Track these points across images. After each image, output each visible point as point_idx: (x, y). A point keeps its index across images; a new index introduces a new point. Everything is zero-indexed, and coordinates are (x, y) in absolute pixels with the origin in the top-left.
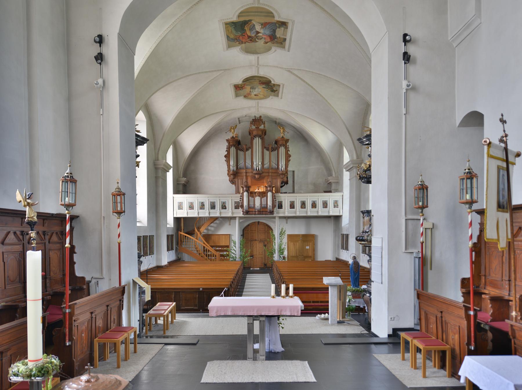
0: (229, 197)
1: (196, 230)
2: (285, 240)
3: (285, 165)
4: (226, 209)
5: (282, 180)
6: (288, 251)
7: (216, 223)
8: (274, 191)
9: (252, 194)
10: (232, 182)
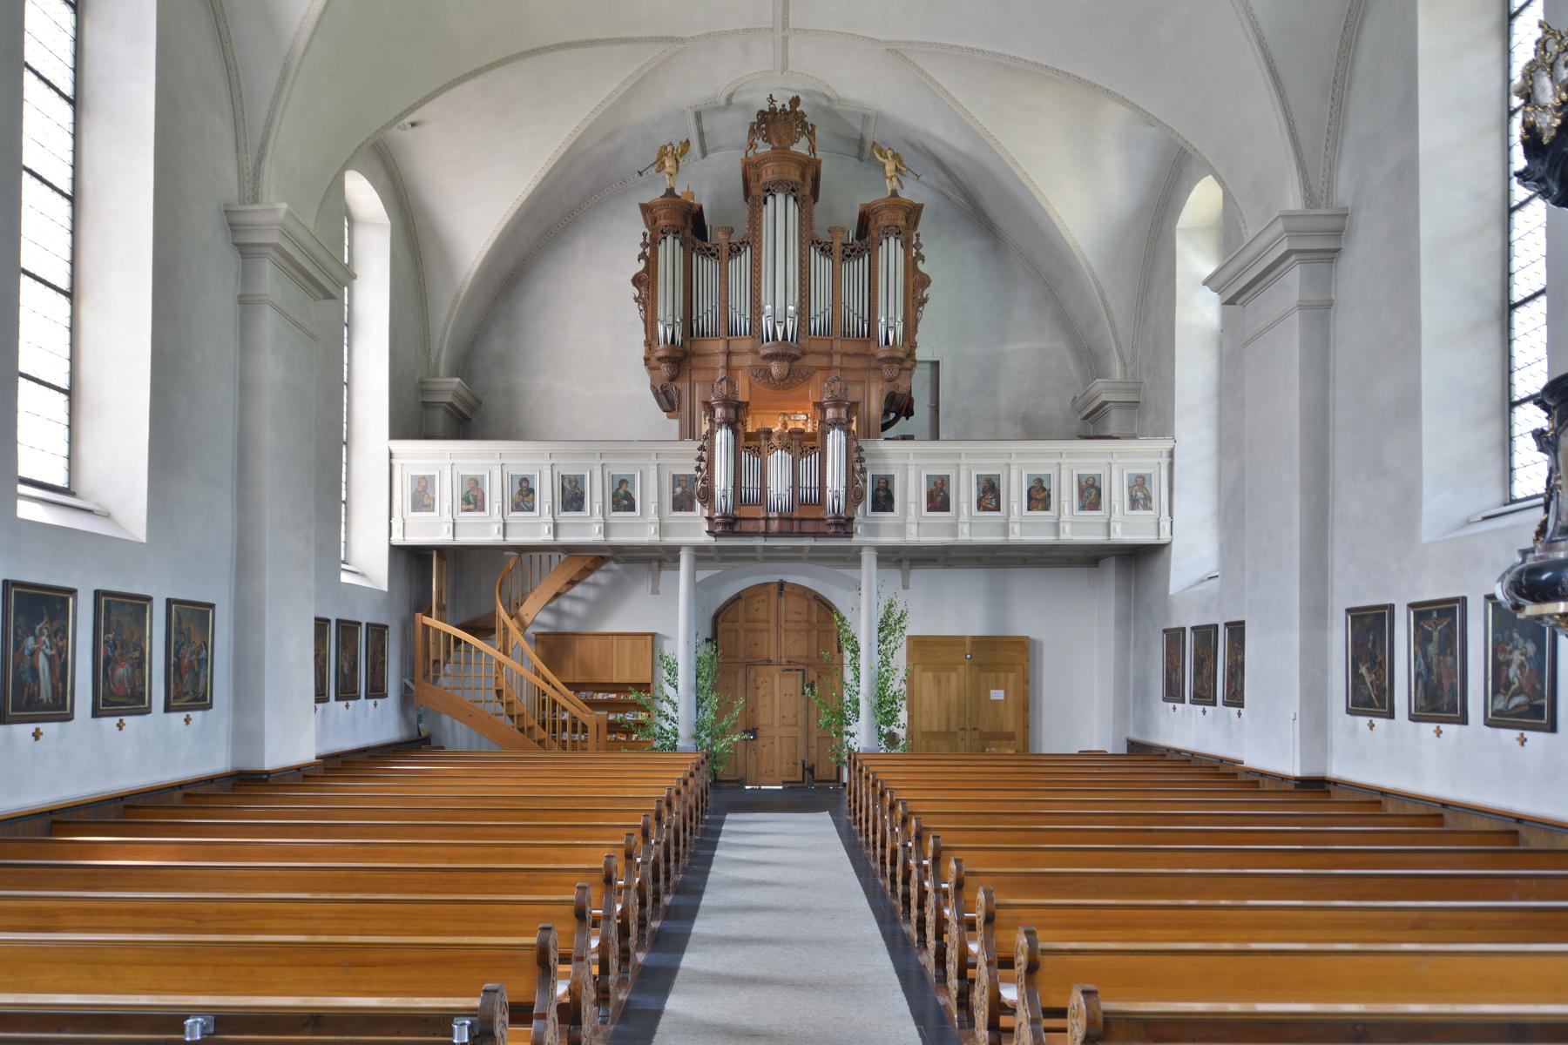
0: (647, 455)
1: (502, 612)
2: (900, 660)
3: (905, 320)
4: (631, 508)
5: (888, 388)
6: (910, 709)
7: (594, 585)
8: (854, 427)
9: (750, 444)
10: (668, 401)
